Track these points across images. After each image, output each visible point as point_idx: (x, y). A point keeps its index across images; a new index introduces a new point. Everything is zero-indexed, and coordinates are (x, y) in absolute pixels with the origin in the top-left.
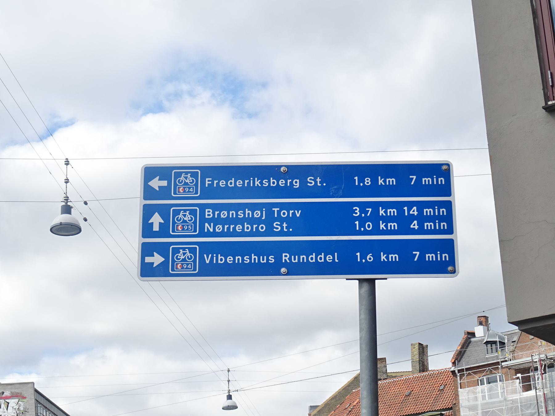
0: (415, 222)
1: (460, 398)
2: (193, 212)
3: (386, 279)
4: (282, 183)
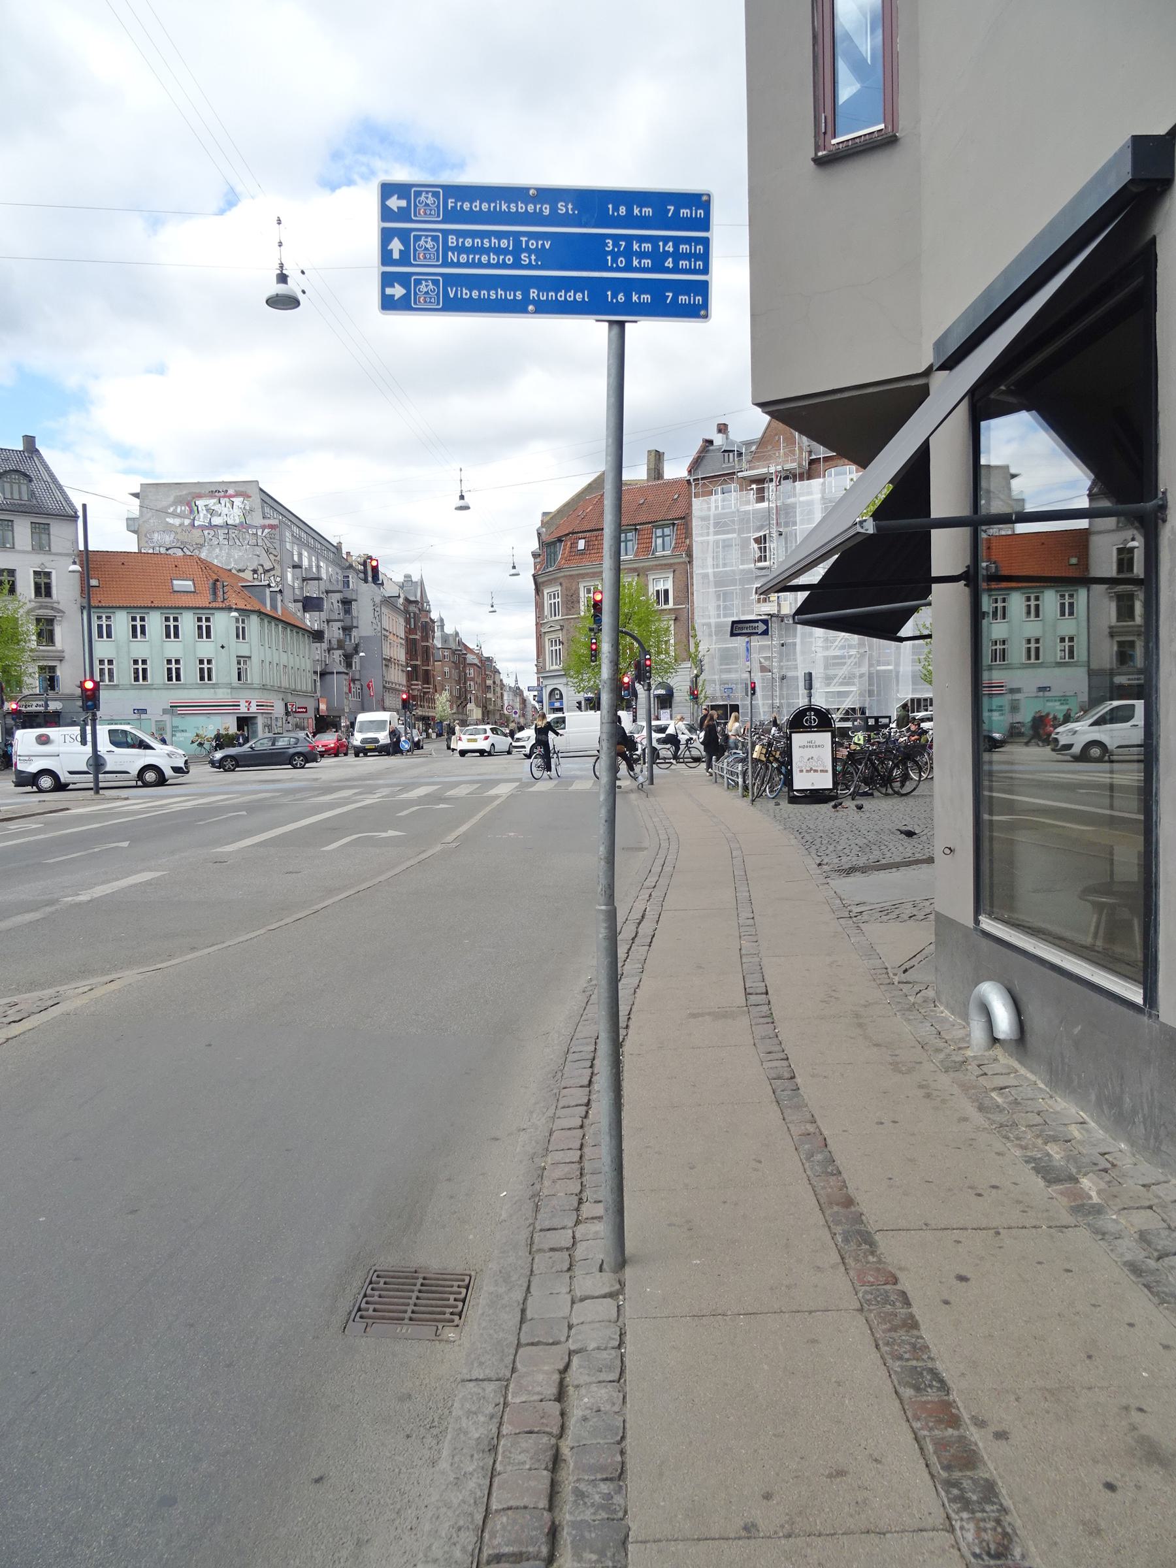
0: (670, 260)
1: (693, 508)
2: (435, 239)
3: (636, 322)
4: (531, 208)
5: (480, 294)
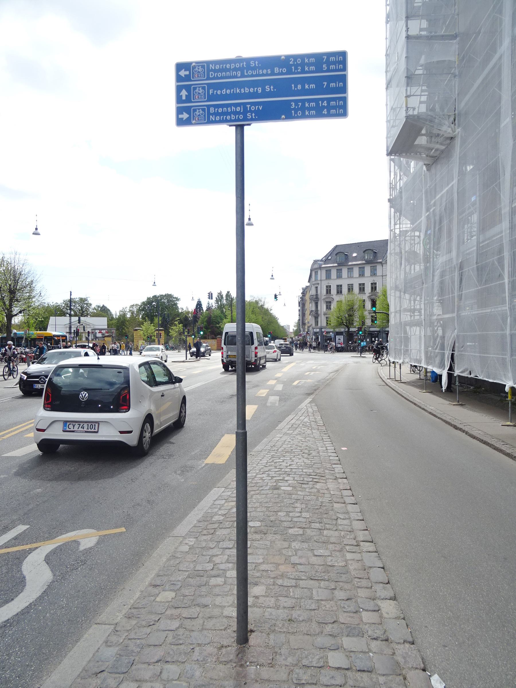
0: (325, 110)
2: (203, 110)
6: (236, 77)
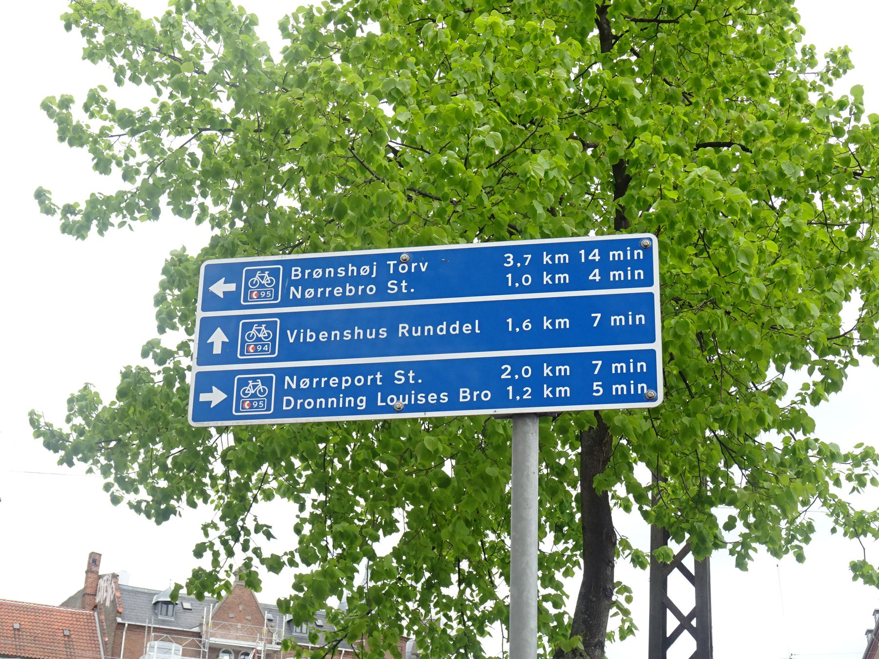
0: (597, 271)
2: (267, 382)
5: (330, 335)
6: (354, 411)
